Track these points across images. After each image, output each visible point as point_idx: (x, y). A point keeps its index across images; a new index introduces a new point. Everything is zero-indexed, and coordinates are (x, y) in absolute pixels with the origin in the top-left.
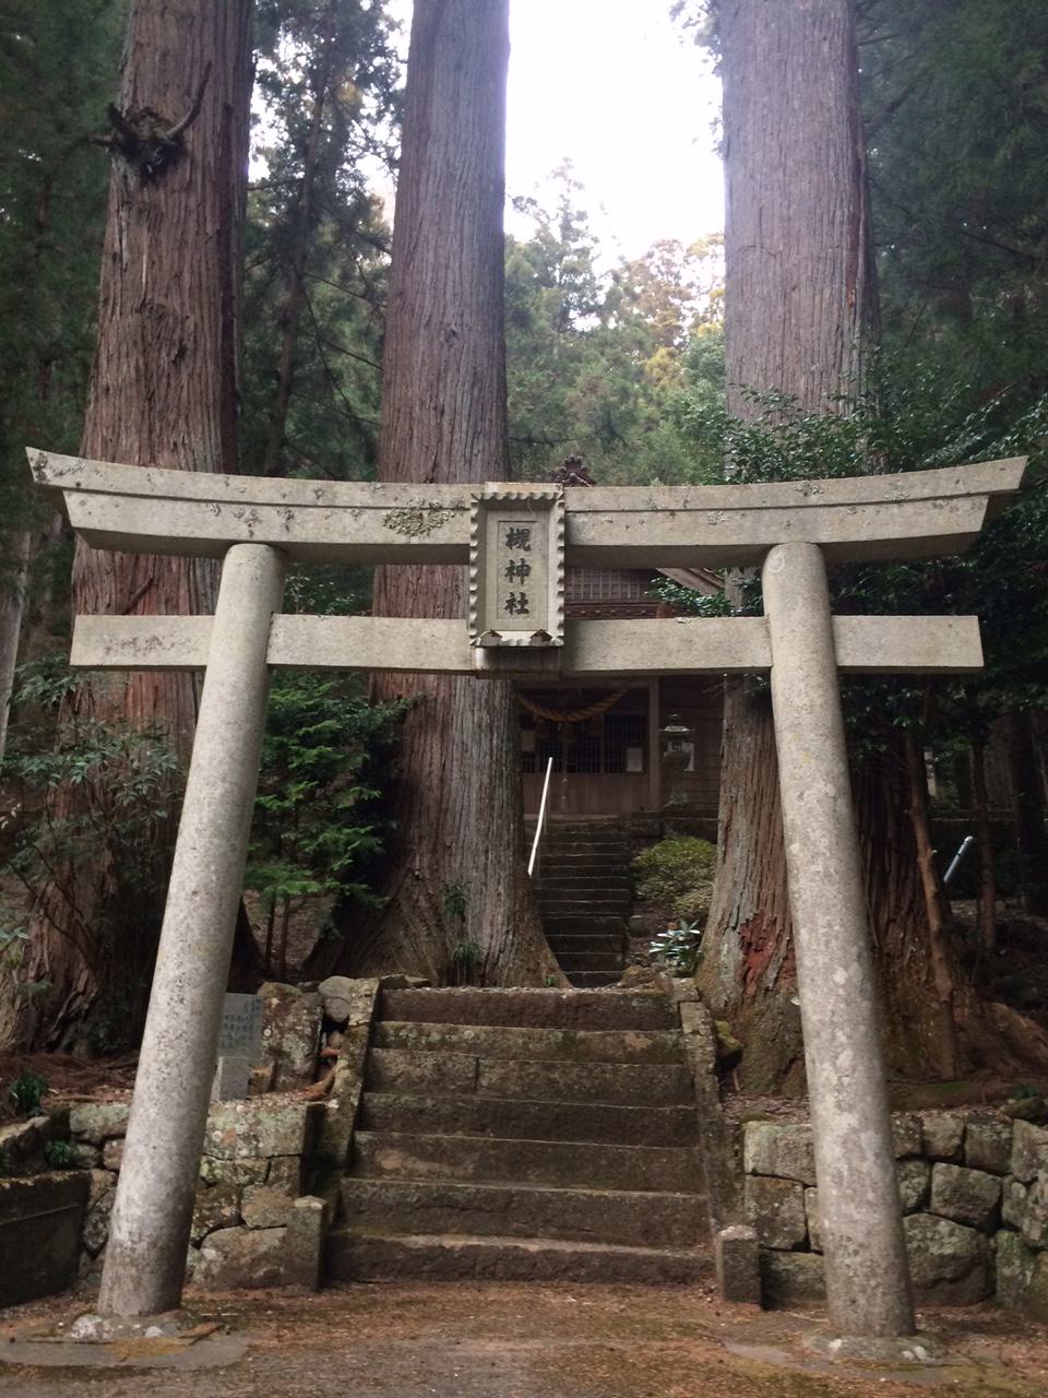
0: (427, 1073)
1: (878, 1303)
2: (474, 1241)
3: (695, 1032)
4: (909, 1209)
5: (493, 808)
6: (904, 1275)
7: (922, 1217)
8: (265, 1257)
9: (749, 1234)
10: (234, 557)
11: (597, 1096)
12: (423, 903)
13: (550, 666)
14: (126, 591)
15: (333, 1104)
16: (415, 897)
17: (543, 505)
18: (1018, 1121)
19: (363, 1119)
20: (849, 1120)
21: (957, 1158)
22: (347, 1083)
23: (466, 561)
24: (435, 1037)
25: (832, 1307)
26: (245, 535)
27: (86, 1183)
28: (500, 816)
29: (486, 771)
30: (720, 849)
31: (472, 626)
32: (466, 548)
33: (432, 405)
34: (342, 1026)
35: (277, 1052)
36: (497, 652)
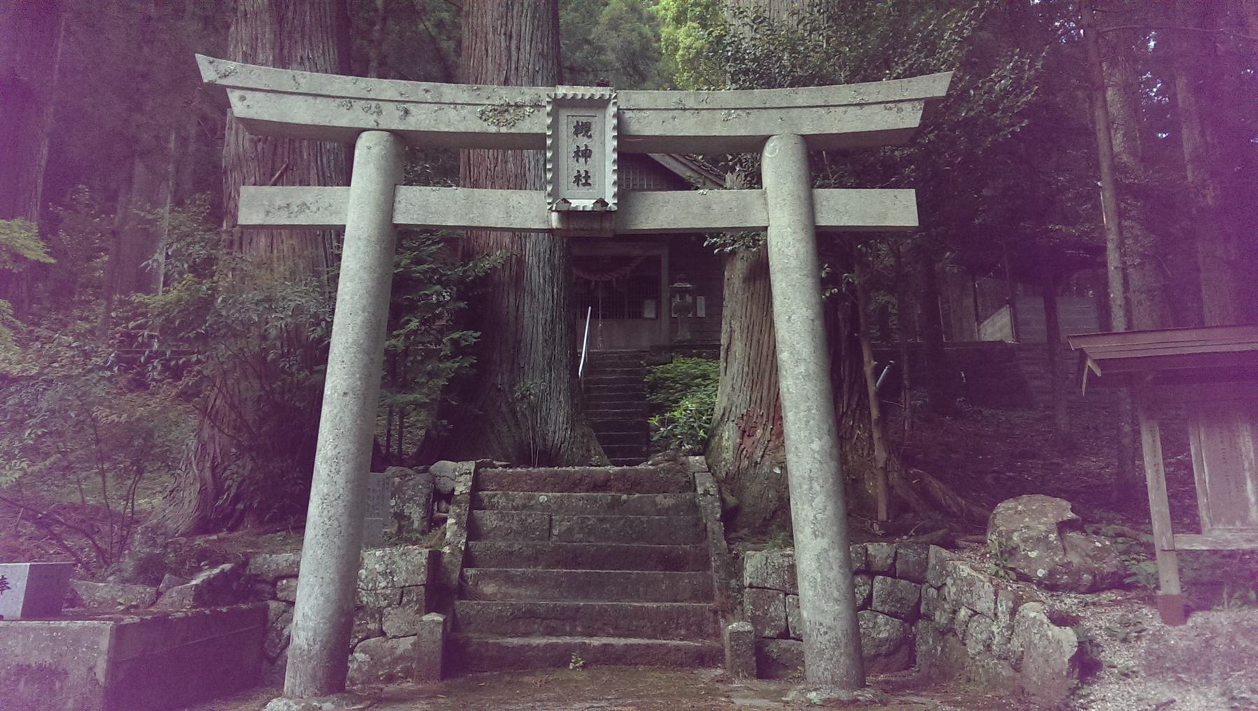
1: (842, 664)
2: (554, 640)
4: (860, 606)
6: (859, 647)
7: (866, 614)
8: (402, 658)
9: (748, 627)
10: (363, 142)
11: (637, 540)
12: (504, 409)
13: (607, 225)
15: (447, 550)
17: (602, 104)
18: (932, 547)
19: (469, 559)
20: (823, 543)
21: (890, 572)
22: (454, 534)
23: (544, 147)
25: (808, 673)
26: (372, 124)
27: (266, 609)
30: (722, 365)
31: (549, 195)
32: (544, 136)
34: (449, 497)
35: (400, 516)
36: (569, 215)
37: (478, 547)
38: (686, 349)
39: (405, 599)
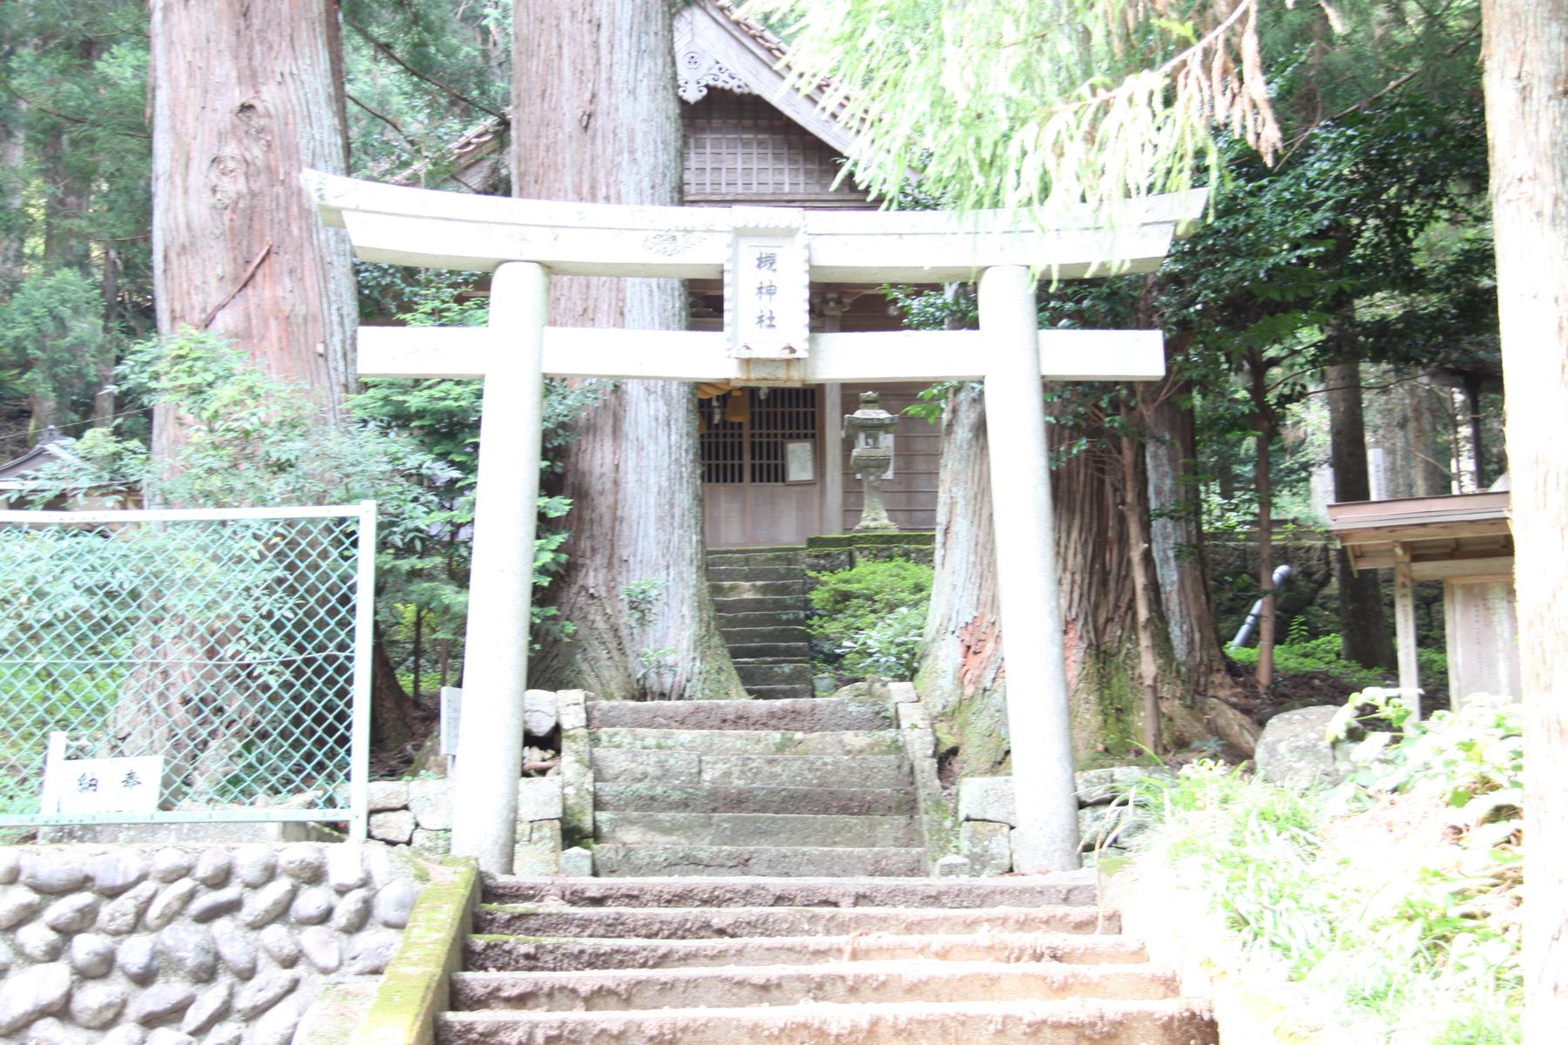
0: (650, 770)
3: (914, 726)
5: (673, 517)
12: (601, 624)
14: (240, 261)
16: (591, 617)
17: (790, 233)
24: (651, 741)
28: (681, 526)
29: (665, 473)
33: (586, 17)
37: (607, 790)
38: (883, 546)
39: (535, 836)
